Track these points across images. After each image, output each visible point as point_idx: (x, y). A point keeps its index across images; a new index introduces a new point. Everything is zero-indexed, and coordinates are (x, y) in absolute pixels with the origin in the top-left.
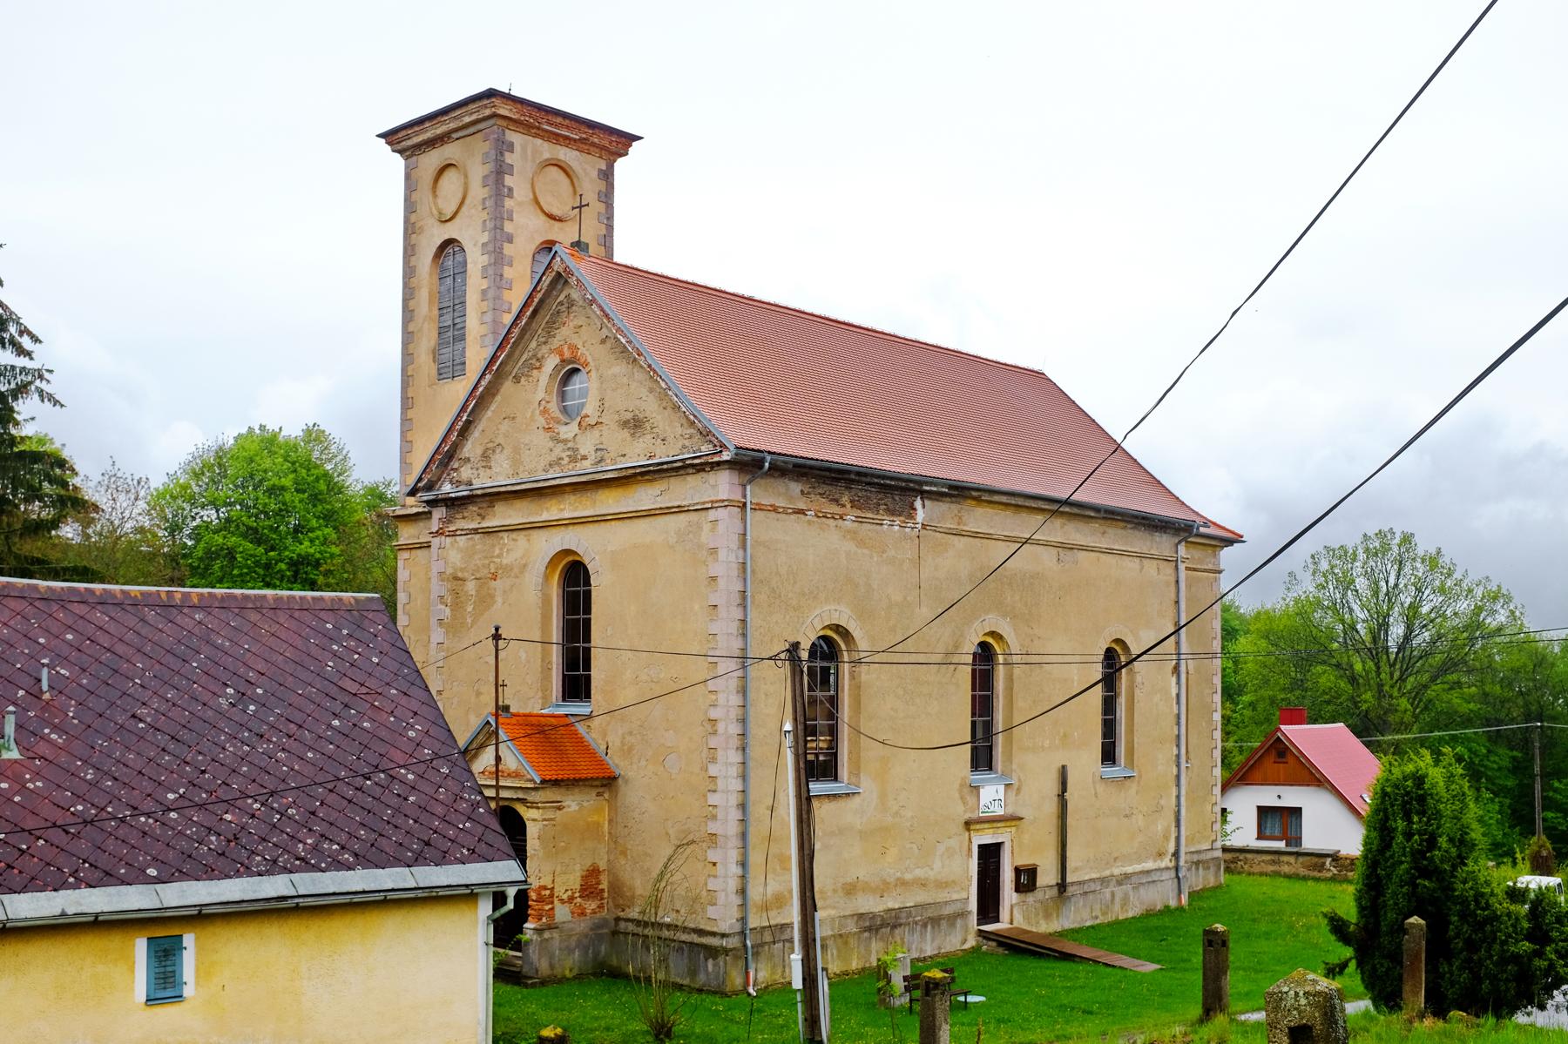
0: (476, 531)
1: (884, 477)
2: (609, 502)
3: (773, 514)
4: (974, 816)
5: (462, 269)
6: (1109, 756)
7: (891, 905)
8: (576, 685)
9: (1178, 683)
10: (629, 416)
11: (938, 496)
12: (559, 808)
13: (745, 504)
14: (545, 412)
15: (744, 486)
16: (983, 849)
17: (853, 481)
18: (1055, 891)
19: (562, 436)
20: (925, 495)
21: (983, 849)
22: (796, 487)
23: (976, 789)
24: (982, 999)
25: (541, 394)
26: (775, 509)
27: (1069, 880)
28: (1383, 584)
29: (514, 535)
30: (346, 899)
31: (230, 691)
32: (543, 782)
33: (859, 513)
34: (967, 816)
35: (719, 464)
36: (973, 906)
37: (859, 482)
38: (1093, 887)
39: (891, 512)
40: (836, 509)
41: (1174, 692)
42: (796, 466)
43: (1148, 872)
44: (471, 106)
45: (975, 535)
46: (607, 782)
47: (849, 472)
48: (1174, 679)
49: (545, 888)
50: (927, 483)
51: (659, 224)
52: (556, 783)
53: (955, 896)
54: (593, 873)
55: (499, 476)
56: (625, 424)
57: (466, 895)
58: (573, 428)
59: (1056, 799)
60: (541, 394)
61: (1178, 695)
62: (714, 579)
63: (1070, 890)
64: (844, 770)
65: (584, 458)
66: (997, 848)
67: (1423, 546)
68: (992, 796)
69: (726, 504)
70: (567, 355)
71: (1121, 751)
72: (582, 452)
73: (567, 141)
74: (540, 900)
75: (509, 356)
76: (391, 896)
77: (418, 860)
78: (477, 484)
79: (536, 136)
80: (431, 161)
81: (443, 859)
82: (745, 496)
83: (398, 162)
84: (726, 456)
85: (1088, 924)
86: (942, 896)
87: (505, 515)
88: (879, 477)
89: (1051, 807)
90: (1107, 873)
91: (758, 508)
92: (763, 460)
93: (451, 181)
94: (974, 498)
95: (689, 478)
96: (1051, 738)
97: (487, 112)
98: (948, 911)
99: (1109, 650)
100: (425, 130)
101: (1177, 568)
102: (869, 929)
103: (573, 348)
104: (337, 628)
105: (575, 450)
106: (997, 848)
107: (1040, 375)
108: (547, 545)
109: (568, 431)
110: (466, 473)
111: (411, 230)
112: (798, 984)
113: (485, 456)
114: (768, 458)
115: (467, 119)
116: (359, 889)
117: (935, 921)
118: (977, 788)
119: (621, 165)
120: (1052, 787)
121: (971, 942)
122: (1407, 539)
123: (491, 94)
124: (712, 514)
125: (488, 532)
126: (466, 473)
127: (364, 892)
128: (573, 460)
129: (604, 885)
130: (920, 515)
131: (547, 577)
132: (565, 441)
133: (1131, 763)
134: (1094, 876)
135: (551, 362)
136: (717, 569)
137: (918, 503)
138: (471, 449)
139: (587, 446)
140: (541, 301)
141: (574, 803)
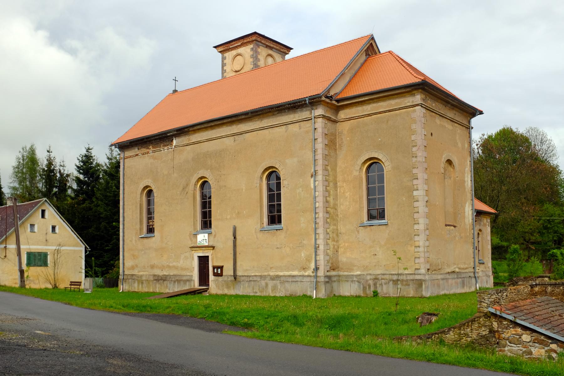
7: (165, 273)
18: (233, 278)
43: (250, 276)
48: (312, 179)
53: (188, 274)
90: (266, 274)
98: (184, 278)
114: (307, 99)
123: (255, 33)
134: (257, 274)
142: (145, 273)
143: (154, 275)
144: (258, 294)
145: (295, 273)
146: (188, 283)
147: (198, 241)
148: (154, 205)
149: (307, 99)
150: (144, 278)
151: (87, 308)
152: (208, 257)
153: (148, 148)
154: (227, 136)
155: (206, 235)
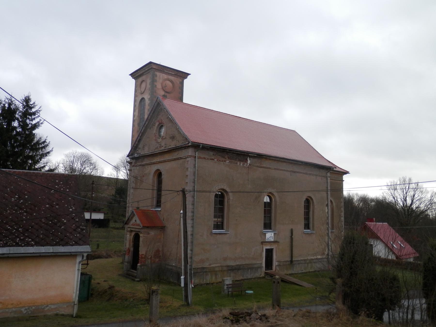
0: (140, 165)
1: (237, 151)
2: (167, 157)
3: (204, 160)
4: (264, 241)
5: (145, 104)
6: (307, 226)
7: (238, 263)
8: (159, 204)
9: (328, 208)
10: (172, 136)
11: (254, 157)
12: (149, 234)
13: (196, 157)
14: (155, 136)
15: (196, 152)
16: (267, 250)
17: (228, 152)
18: (289, 263)
19: (159, 141)
20: (250, 157)
21: (267, 250)
22: (211, 153)
23: (265, 234)
24: (252, 292)
25: (155, 132)
26: (205, 158)
27: (293, 260)
28: (404, 190)
29: (148, 166)
30: (50, 254)
31: (17, 196)
32: (143, 227)
33: (230, 160)
34: (262, 241)
35: (189, 146)
36: (264, 265)
37: (230, 153)
38: (302, 262)
39: (240, 161)
40: (224, 159)
41: (327, 211)
42: (210, 147)
43: (299, 261)
44: (147, 66)
45: (264, 167)
46: (163, 228)
47: (227, 150)
48: (326, 208)
49: (143, 255)
50: (250, 153)
51: (194, 94)
52: (148, 227)
53: (258, 262)
54: (158, 251)
55: (146, 151)
56: (171, 138)
57: (72, 256)
58: (161, 139)
59: (290, 237)
60: (155, 132)
61: (328, 212)
62: (187, 176)
63: (294, 263)
64: (225, 227)
65: (162, 146)
66: (272, 250)
67: (414, 181)
68: (270, 236)
69: (190, 156)
70: (160, 122)
71: (311, 225)
72: (162, 145)
73: (172, 75)
74: (142, 258)
75: (148, 123)
76: (73, 254)
77: (57, 244)
78: (141, 154)
79: (163, 73)
80: (140, 79)
81: (66, 244)
82: (196, 155)
83: (134, 81)
84: (190, 144)
85: (300, 272)
86: (254, 262)
87: (146, 161)
88: (235, 151)
89: (288, 240)
90: (306, 258)
91: (199, 158)
92: (200, 145)
93: (143, 85)
94: (265, 158)
95: (183, 150)
96: (290, 220)
97: (150, 67)
98: (256, 266)
99: (307, 199)
100: (138, 73)
101: (327, 179)
102: (230, 270)
103: (162, 120)
104: (60, 182)
105: (161, 145)
106: (272, 250)
107: (294, 131)
108: (154, 168)
109: (160, 140)
110: (140, 151)
111: (136, 96)
112: (183, 285)
113: (143, 147)
114: (201, 145)
115: (146, 69)
116: (32, 252)
117: (252, 269)
118: (265, 234)
119: (185, 81)
120: (289, 234)
121: (263, 275)
122: (410, 180)
123: (151, 63)
124: (187, 159)
125: (143, 165)
126: (140, 151)
127: (33, 253)
128: (160, 147)
129: (161, 254)
130: (249, 162)
131: (154, 176)
132: (159, 143)
133: (313, 229)
134: (302, 259)
135: (157, 124)
136: (188, 173)
137: (248, 159)
138: (141, 146)
139: (163, 144)
140: (155, 109)
141: (152, 233)
142: (217, 265)
143: (228, 266)
144: (303, 271)
145: (319, 257)
146: (259, 269)
147: (267, 237)
148: (305, 205)
149: (201, 145)
150: (217, 269)
151: (93, 325)
152: (266, 249)
153: (224, 157)
154: (287, 171)
155: (273, 234)
